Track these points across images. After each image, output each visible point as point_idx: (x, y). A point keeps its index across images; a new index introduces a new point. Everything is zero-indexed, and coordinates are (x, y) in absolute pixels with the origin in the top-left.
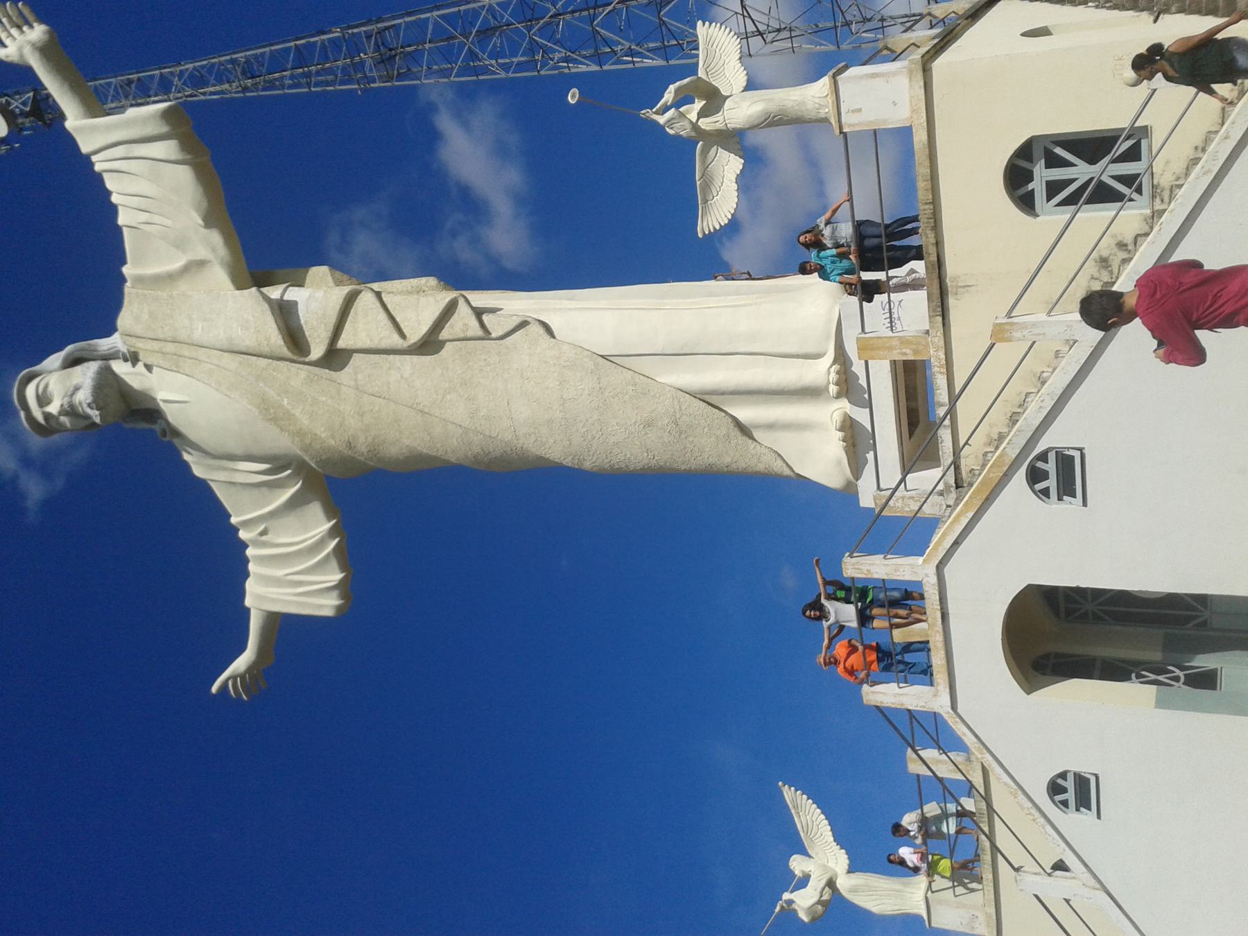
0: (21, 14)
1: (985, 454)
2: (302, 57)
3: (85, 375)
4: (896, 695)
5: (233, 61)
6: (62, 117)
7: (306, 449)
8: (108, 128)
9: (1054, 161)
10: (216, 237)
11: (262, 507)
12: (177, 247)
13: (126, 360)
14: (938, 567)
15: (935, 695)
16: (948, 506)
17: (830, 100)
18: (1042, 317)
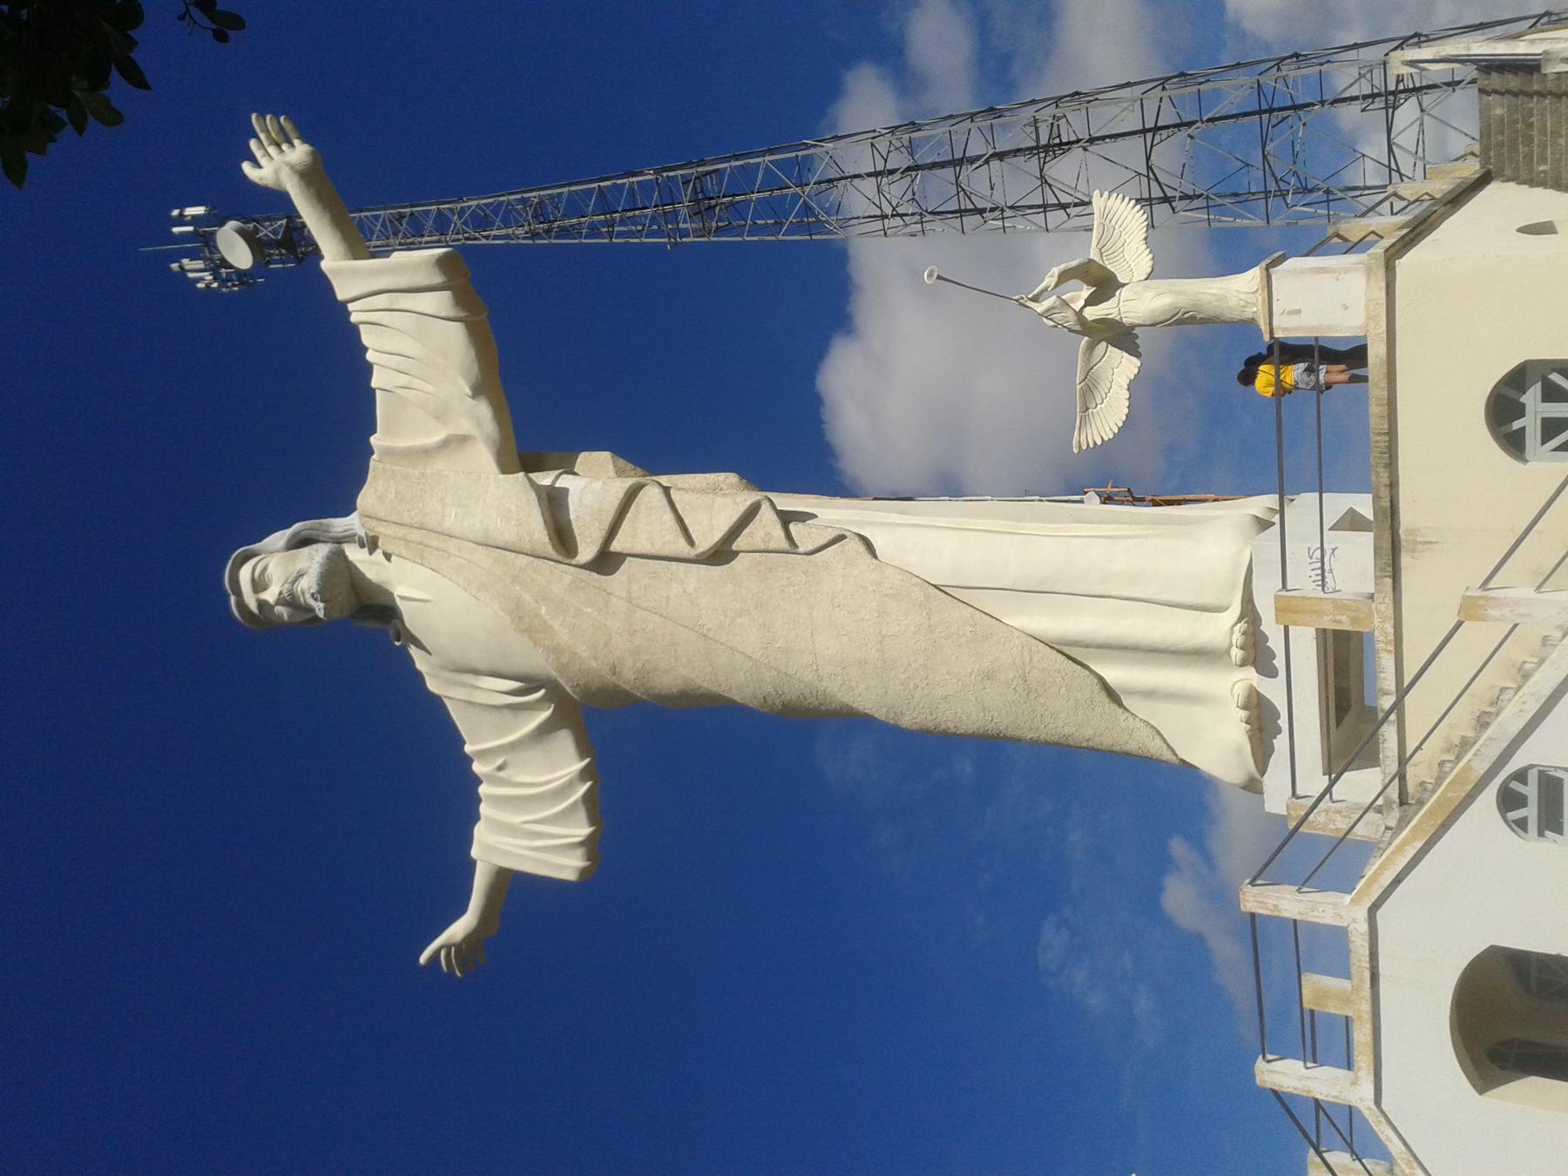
0: (282, 129)
1: (1442, 764)
2: (605, 203)
3: (313, 559)
4: (1300, 1078)
5: (523, 201)
6: (317, 255)
7: (562, 669)
8: (372, 273)
9: (1552, 394)
10: (483, 409)
11: (505, 736)
12: (437, 418)
13: (362, 546)
14: (1370, 910)
15: (1353, 1084)
16: (1387, 828)
17: (1261, 297)
18: (1529, 592)
